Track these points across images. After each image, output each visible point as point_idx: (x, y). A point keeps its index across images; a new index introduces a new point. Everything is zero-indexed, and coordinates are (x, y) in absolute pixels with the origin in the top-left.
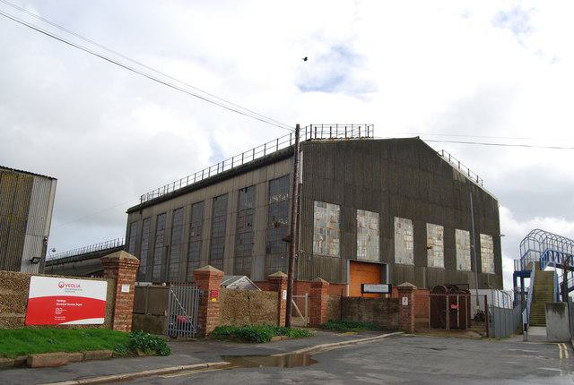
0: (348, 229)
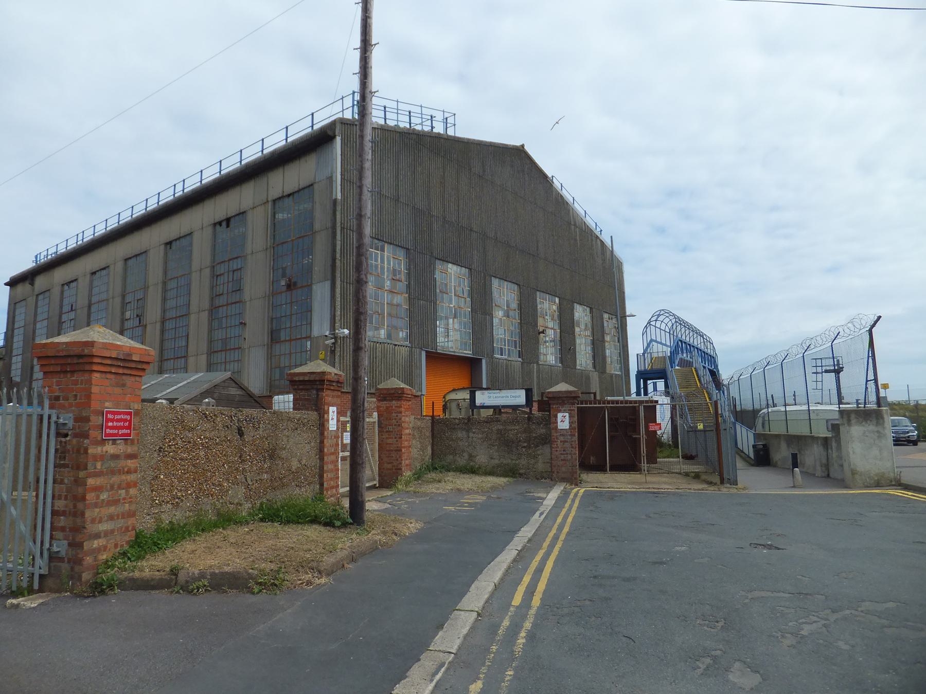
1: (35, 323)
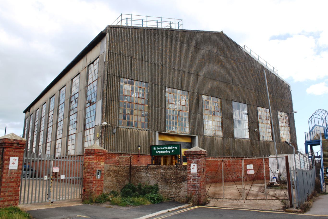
0: (196, 112)
1: (48, 128)
